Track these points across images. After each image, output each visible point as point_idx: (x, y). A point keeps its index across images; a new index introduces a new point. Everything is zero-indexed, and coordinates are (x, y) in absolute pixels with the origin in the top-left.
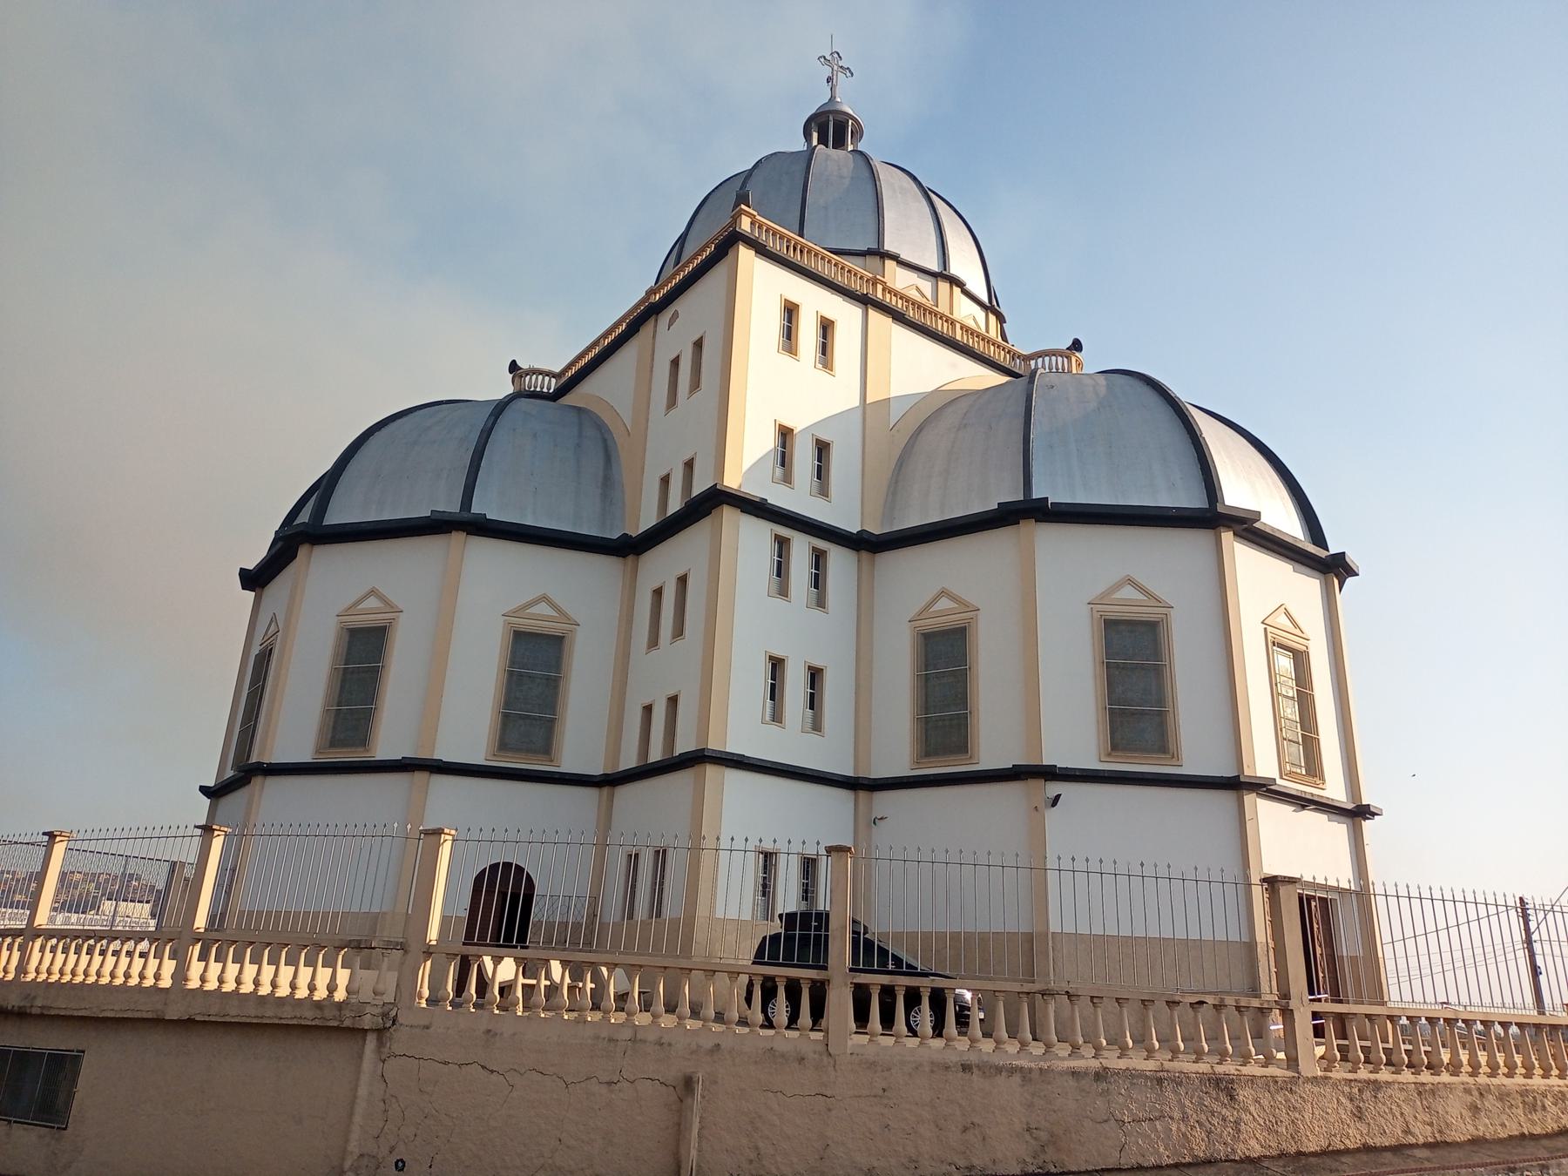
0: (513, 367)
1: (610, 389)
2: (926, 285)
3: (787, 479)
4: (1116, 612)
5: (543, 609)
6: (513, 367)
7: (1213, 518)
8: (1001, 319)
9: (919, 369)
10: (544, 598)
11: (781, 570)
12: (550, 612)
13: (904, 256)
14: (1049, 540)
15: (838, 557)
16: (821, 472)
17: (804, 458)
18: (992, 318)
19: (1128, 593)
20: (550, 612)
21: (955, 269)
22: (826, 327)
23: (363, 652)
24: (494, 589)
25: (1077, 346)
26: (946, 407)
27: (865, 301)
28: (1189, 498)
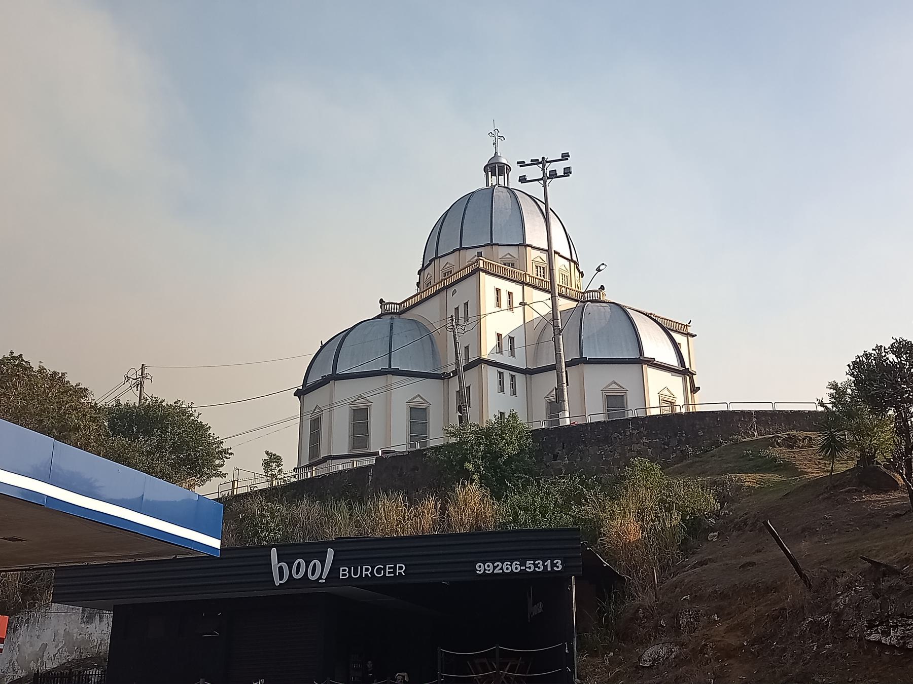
0: (381, 301)
3: (501, 352)
4: (611, 393)
5: (418, 399)
6: (381, 301)
7: (641, 361)
8: (576, 263)
11: (501, 383)
12: (668, 394)
13: (534, 245)
14: (588, 369)
15: (519, 377)
16: (512, 348)
18: (572, 264)
19: (614, 386)
20: (668, 394)
22: (510, 294)
23: (360, 418)
24: (404, 393)
25: (602, 288)
27: (523, 283)
28: (635, 355)
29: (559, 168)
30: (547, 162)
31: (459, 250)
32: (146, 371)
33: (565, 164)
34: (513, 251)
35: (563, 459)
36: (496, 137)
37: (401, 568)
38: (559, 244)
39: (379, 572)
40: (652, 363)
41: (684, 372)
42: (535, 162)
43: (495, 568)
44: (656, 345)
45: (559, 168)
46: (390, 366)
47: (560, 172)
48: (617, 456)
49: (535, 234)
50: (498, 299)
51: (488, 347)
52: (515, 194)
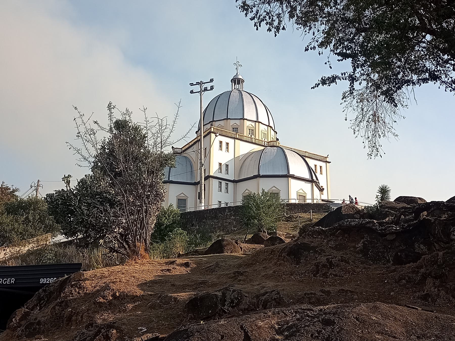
1: (191, 153)
2: (253, 124)
5: (182, 195)
7: (288, 176)
9: (244, 148)
10: (182, 193)
11: (220, 187)
13: (248, 119)
14: (172, 186)
15: (230, 184)
16: (227, 170)
17: (224, 168)
18: (269, 128)
19: (274, 188)
21: (270, 125)
22: (227, 144)
26: (250, 154)
28: (285, 173)
29: (208, 86)
30: (203, 83)
31: (212, 122)
32: (40, 183)
33: (211, 84)
34: (238, 122)
35: (196, 226)
36: (238, 65)
37: (13, 280)
38: (263, 118)
39: (5, 282)
40: (293, 177)
41: (313, 181)
42: (198, 83)
43: (47, 281)
44: (297, 167)
45: (208, 86)
46: (169, 179)
47: (209, 88)
48: (220, 225)
49: (249, 114)
50: (221, 146)
51: (214, 170)
52: (241, 93)
